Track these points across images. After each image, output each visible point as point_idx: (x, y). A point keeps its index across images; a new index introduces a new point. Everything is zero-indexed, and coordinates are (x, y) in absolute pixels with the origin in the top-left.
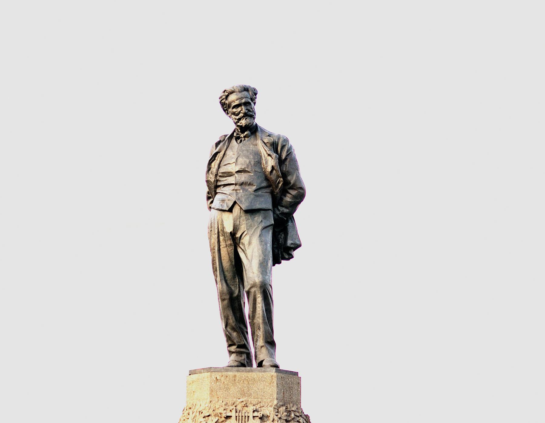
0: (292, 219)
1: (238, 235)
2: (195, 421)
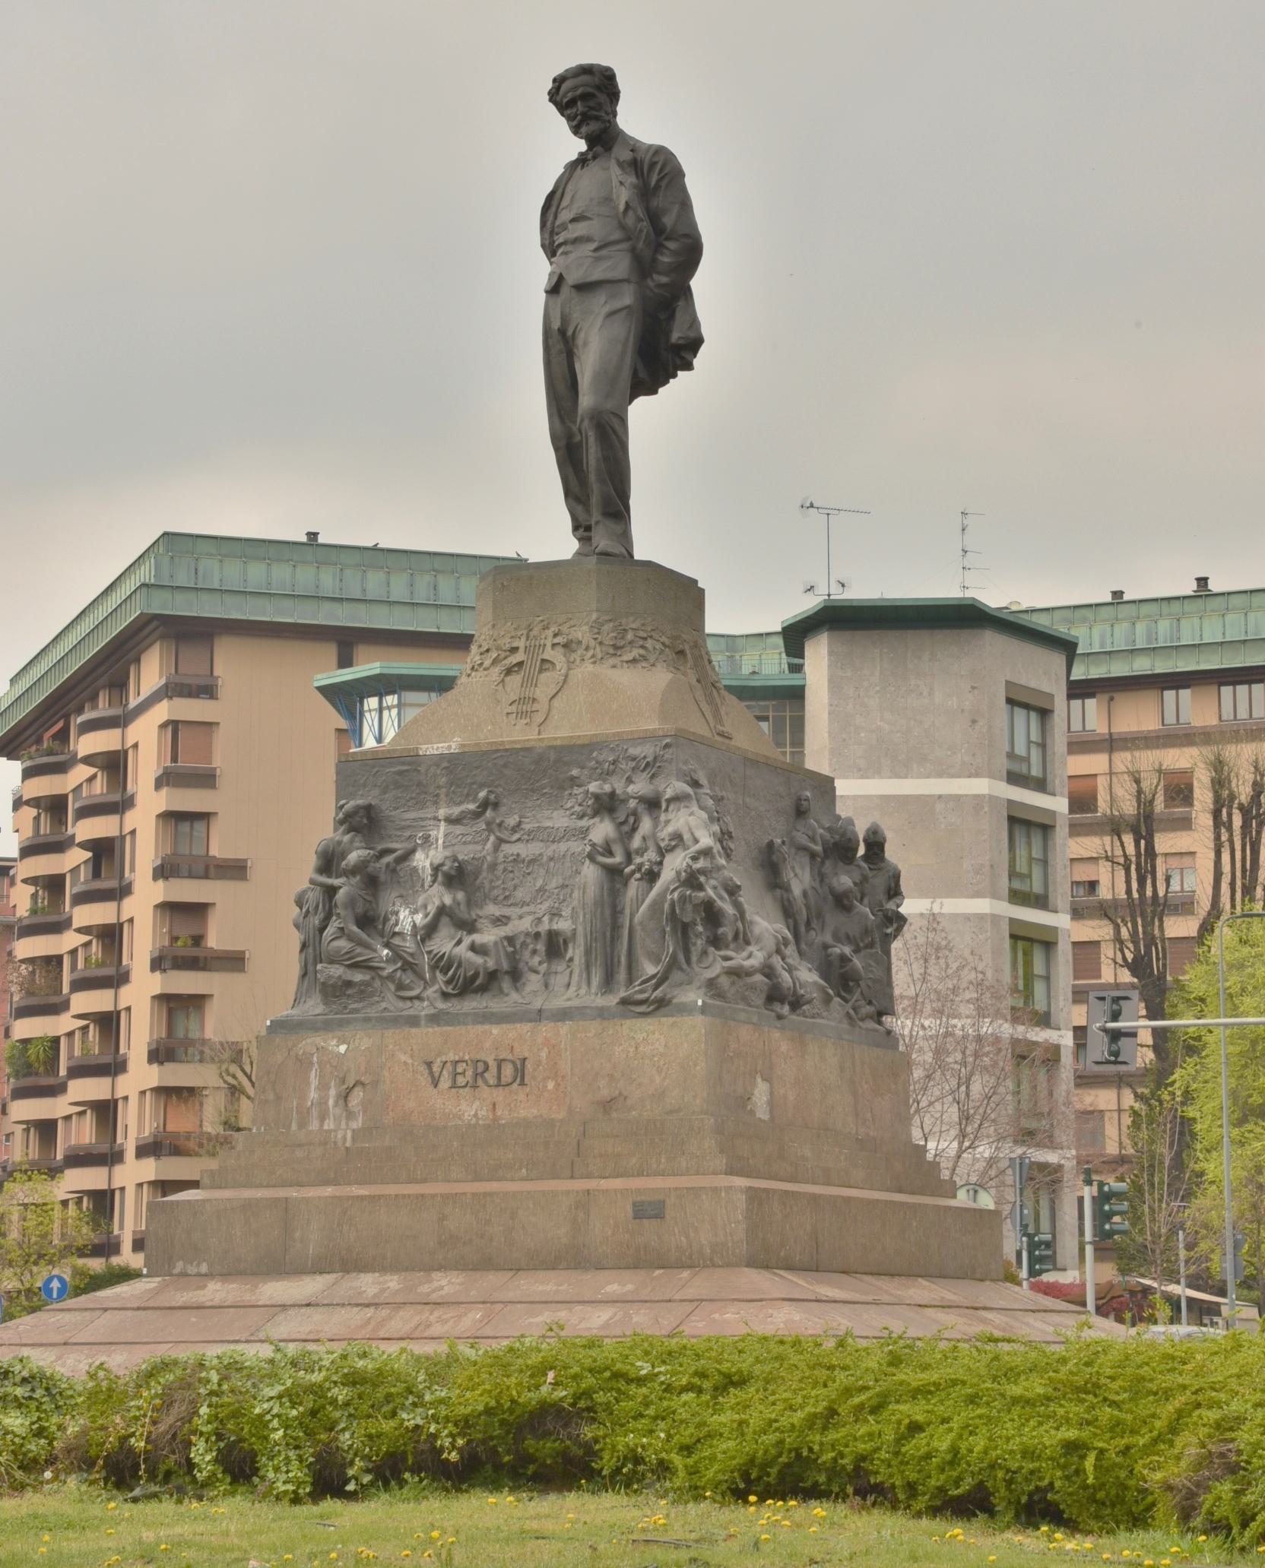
0: (687, 293)
1: (570, 333)
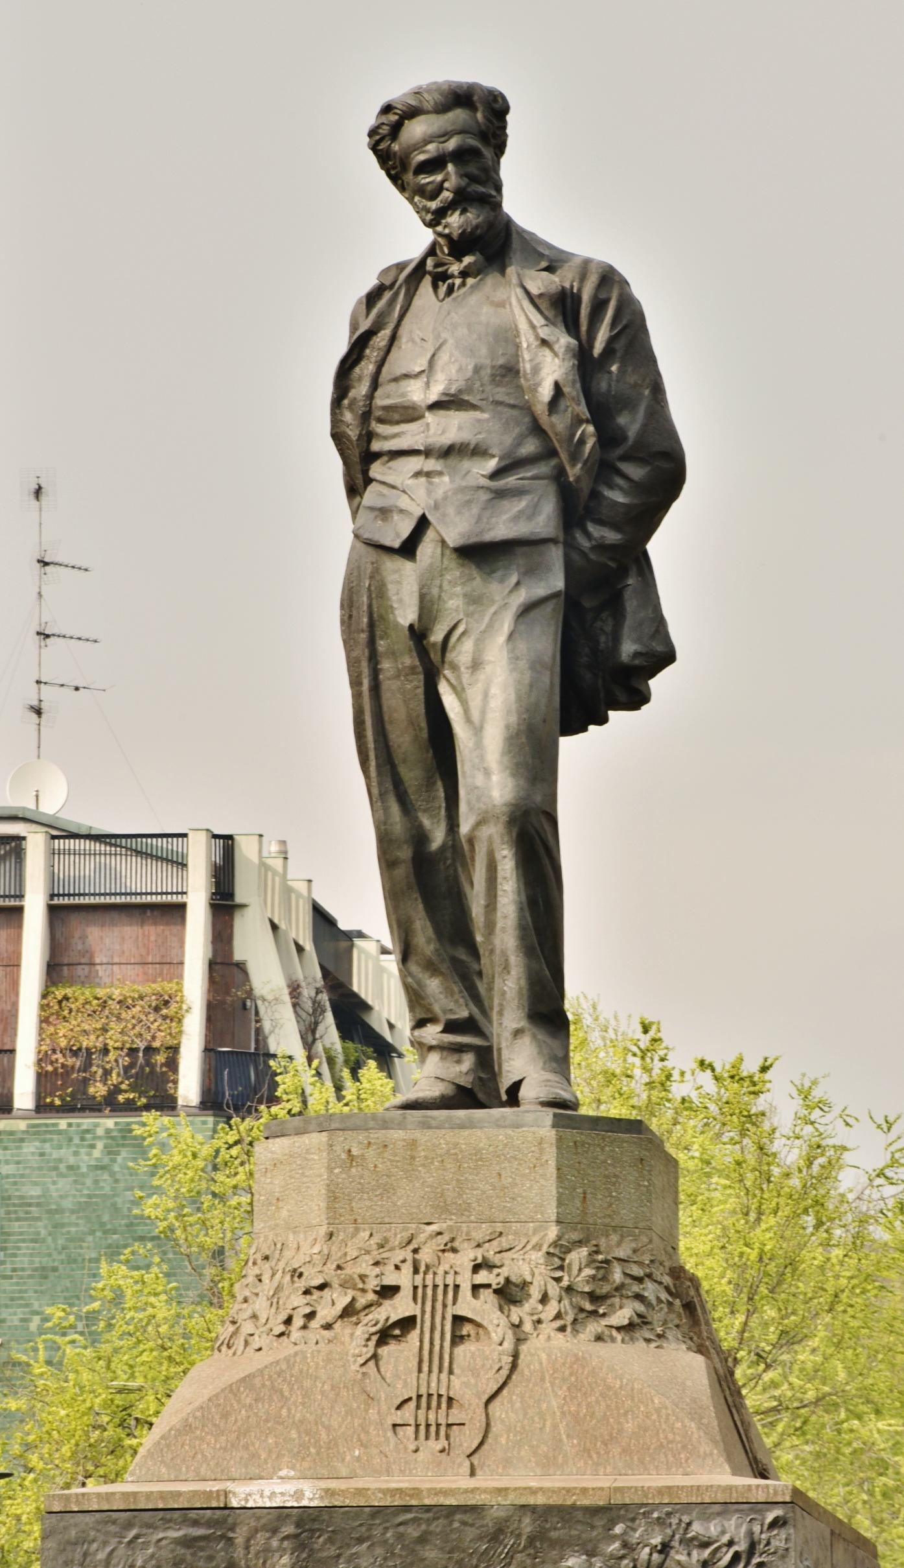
0: (643, 564)
1: (437, 637)
2: (278, 1303)
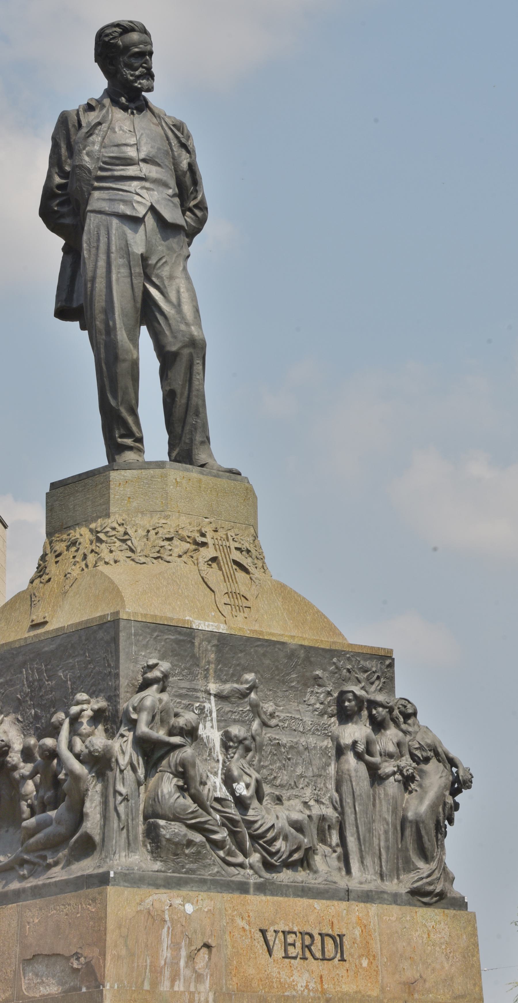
1: (152, 261)
